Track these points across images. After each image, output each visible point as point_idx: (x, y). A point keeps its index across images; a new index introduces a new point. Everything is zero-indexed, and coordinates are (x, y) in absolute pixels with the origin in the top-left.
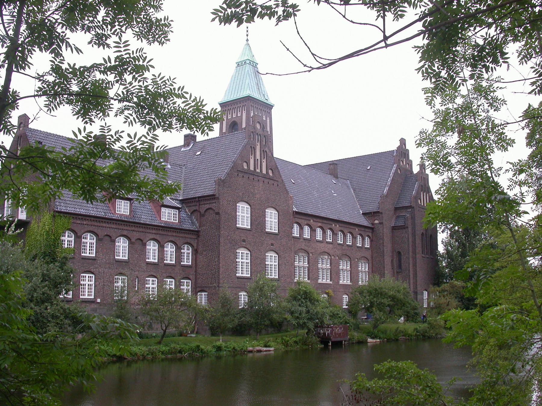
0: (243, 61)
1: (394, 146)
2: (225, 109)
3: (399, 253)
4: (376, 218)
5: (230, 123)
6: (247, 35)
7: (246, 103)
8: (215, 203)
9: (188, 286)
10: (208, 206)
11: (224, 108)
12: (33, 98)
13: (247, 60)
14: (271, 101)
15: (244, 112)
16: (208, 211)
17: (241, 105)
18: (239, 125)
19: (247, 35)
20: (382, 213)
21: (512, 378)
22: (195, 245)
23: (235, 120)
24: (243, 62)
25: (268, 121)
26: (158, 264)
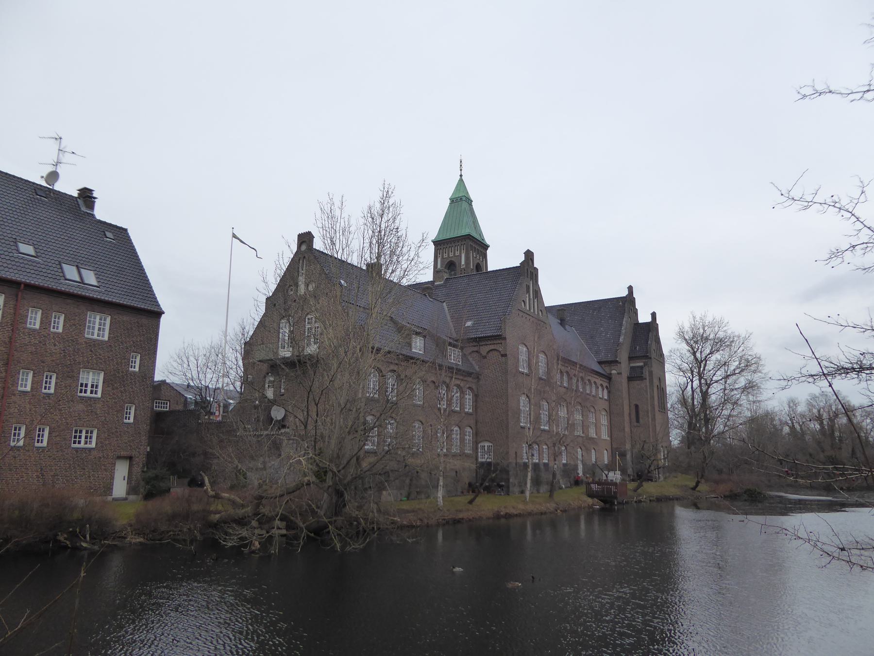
0: (459, 197)
1: (624, 293)
2: (439, 247)
3: (637, 406)
4: (613, 368)
5: (446, 263)
6: (461, 170)
7: (465, 242)
8: (501, 343)
9: (457, 435)
10: (492, 347)
11: (439, 246)
12: (832, 88)
13: (463, 196)
14: (488, 241)
15: (462, 251)
16: (493, 352)
17: (441, 247)
18: (457, 266)
19: (461, 170)
20: (620, 363)
21: (468, 494)
22: (475, 390)
23: (453, 259)
24: (459, 199)
25: (484, 262)
26: (460, 413)
